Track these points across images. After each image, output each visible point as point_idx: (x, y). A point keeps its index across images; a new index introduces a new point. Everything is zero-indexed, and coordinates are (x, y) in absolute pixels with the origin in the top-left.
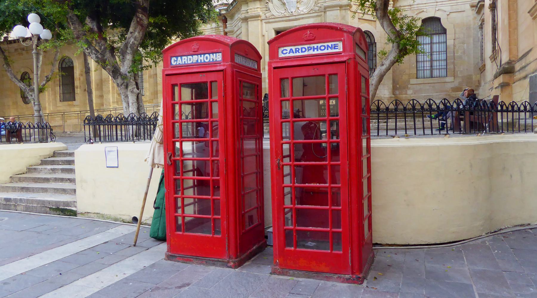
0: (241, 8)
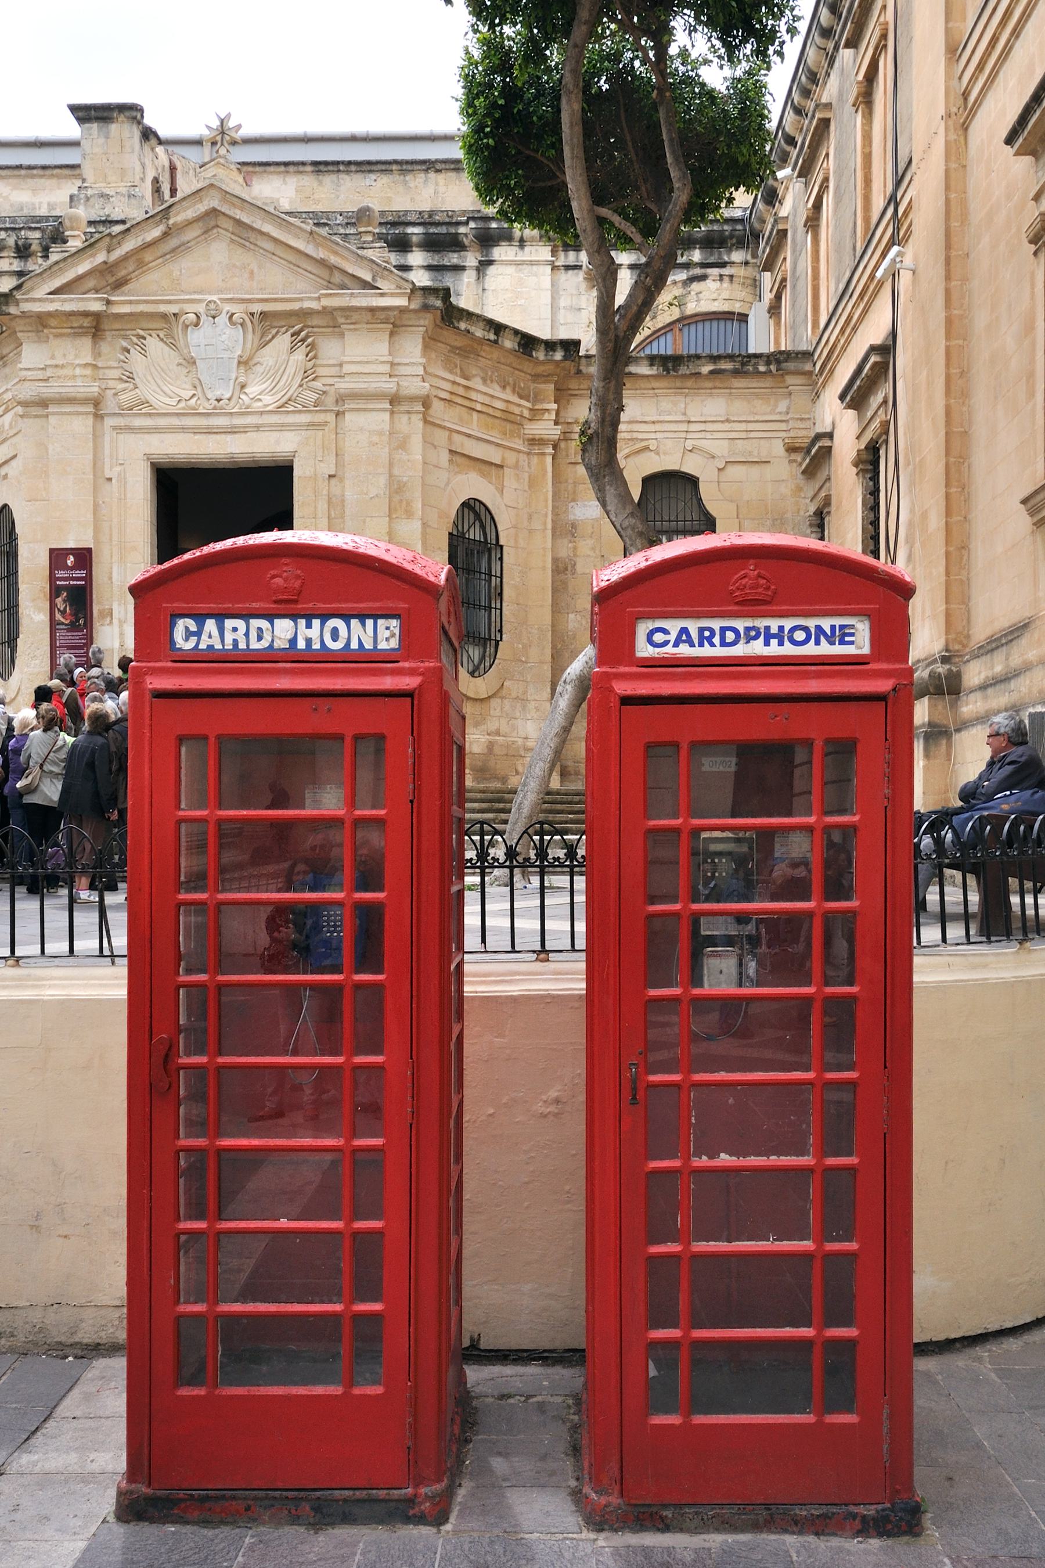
0: (19, 354)
